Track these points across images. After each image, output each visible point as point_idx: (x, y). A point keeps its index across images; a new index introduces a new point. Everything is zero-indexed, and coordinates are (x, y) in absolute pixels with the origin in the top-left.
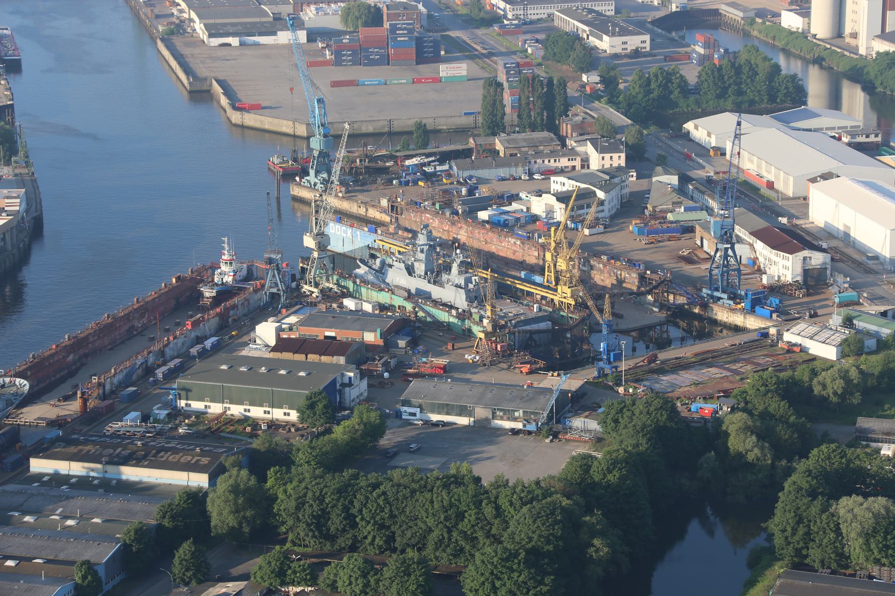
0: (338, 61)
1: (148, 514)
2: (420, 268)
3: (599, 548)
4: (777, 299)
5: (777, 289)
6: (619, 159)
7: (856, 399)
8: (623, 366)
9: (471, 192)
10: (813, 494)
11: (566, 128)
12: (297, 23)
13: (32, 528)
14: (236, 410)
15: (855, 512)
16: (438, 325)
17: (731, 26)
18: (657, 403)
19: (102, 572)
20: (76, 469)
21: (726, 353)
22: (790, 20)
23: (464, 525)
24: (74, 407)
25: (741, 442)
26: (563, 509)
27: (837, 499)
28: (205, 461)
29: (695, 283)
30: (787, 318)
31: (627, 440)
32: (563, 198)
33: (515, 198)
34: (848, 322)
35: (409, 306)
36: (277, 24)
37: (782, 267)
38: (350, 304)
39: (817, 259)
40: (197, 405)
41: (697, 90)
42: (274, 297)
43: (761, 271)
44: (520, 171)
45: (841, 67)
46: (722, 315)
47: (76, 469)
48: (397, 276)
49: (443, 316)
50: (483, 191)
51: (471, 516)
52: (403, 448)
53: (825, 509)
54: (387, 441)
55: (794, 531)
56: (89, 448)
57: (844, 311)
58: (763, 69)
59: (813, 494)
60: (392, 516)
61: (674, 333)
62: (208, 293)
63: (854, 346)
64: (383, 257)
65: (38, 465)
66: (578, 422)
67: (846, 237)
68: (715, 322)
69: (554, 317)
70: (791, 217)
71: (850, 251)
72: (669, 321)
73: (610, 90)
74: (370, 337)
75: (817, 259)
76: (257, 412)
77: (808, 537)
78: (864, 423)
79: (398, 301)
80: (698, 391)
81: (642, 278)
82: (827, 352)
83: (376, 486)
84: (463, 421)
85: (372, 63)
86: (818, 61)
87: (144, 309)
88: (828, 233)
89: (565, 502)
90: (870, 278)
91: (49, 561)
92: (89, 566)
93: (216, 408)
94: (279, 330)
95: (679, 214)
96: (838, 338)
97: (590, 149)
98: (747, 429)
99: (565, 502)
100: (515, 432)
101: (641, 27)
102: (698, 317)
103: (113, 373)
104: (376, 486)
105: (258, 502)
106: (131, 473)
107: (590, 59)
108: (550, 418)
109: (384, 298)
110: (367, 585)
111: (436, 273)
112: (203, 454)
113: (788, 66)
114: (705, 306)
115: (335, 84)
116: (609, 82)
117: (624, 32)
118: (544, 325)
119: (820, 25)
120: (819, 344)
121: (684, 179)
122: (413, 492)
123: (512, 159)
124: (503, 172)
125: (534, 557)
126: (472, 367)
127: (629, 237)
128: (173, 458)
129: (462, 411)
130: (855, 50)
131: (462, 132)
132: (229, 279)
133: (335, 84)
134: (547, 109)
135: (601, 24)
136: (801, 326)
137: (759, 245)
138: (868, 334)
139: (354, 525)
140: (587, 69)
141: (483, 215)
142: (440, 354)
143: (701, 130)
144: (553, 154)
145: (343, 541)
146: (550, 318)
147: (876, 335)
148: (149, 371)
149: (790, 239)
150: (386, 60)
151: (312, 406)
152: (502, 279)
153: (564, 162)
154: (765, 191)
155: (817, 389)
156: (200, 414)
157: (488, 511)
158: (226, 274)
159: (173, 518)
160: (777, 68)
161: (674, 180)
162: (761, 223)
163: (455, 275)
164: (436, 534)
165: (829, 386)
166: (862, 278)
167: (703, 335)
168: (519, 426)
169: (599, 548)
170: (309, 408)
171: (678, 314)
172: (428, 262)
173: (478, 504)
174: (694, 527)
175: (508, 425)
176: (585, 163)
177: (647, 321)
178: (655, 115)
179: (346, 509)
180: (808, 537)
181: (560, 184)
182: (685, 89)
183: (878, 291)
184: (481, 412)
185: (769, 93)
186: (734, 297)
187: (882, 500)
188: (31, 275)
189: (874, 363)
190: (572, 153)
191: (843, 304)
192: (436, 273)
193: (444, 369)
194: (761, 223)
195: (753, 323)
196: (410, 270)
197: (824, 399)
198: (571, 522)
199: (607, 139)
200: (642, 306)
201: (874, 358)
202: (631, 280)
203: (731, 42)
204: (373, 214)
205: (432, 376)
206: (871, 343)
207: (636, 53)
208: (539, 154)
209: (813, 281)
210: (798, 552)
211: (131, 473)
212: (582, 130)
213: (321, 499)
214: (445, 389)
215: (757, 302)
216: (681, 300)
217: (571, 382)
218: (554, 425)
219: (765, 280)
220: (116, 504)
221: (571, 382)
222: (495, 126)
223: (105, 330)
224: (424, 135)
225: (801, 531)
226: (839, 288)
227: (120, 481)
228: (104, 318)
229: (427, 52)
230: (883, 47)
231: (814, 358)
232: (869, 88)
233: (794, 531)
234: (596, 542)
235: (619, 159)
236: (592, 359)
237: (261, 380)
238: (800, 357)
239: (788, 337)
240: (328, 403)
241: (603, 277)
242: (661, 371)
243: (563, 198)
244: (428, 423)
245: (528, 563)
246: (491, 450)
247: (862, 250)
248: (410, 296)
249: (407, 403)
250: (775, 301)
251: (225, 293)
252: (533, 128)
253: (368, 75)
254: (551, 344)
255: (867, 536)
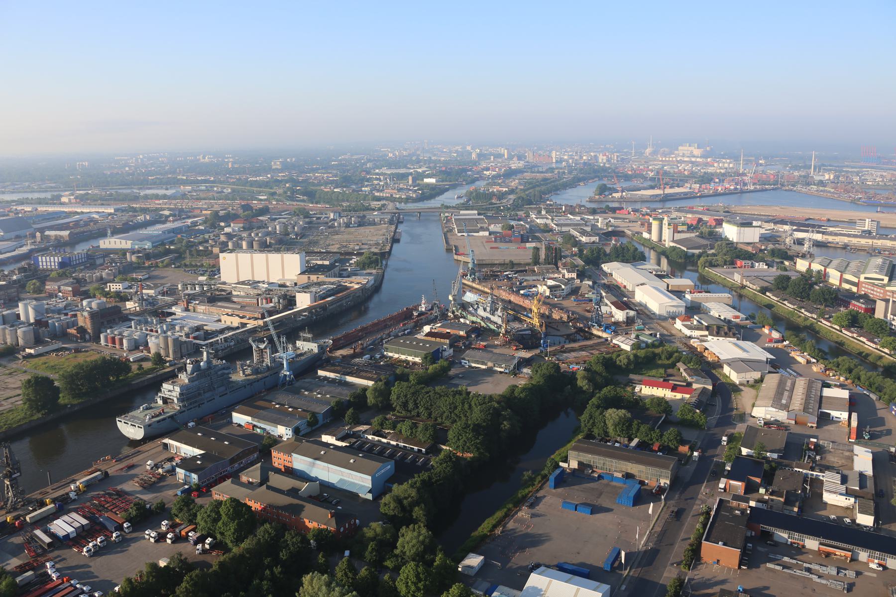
0: (495, 241)
1: (346, 395)
2: (488, 309)
3: (506, 425)
4: (616, 328)
5: (617, 324)
6: (574, 275)
7: (632, 367)
8: (549, 349)
9: (520, 284)
10: (598, 407)
11: (559, 264)
12: (487, 229)
13: (306, 396)
14: (403, 357)
15: (613, 415)
16: (491, 330)
17: (628, 236)
18: (551, 365)
19: (320, 418)
20: (332, 375)
21: (591, 346)
22: (646, 235)
23: (456, 412)
24: (352, 352)
25: (582, 383)
26: (494, 408)
27: (607, 409)
28: (375, 376)
29: (587, 319)
30: (616, 333)
31: (538, 380)
32: (550, 287)
33: (535, 286)
34: (637, 337)
35: (483, 324)
36: (482, 229)
37: (620, 315)
38: (462, 320)
39: (632, 313)
40: (390, 354)
41: (609, 255)
42: (436, 317)
43: (613, 316)
44: (541, 278)
45: (659, 251)
46: (595, 332)
47: (332, 375)
48: (481, 312)
49: (492, 327)
50: (525, 284)
51: (459, 408)
52: (456, 376)
53: (601, 414)
54: (452, 372)
55: (588, 422)
56: (339, 368)
57: (636, 333)
58: (632, 249)
59: (598, 407)
60: (431, 405)
61: (578, 337)
62: (415, 314)
63: (636, 346)
64: (481, 306)
65: (321, 373)
66: (525, 370)
67: (646, 306)
68: (592, 334)
69: (532, 329)
70: (628, 298)
71: (646, 311)
72: (576, 332)
73: (580, 254)
74: (462, 333)
75: (632, 313)
76: (410, 358)
77: (594, 424)
78: (632, 376)
79: (479, 321)
80: (575, 362)
81: (568, 317)
82: (627, 347)
83: (427, 393)
84: (484, 367)
85: (507, 242)
86: (653, 248)
87: (391, 318)
88: (640, 304)
89: (496, 405)
90: (650, 321)
91: (304, 410)
92: (314, 415)
93: (396, 356)
94: (431, 328)
95: (590, 295)
96: (632, 342)
97: (565, 271)
98: (584, 378)
99: (496, 405)
100: (501, 372)
101: (598, 235)
102: (587, 332)
103: (367, 341)
104: (427, 393)
105: (383, 393)
106: (349, 379)
107: (577, 243)
108: (514, 368)
109: (474, 319)
110: (412, 433)
111: (493, 311)
112: (376, 373)
113: (641, 249)
114: (589, 328)
115: (492, 248)
116: (581, 251)
117: (590, 236)
118: (529, 332)
119: (654, 237)
120: (625, 344)
121: (594, 283)
122: (441, 396)
123: (539, 274)
124: (534, 278)
125: (477, 428)
126: (496, 346)
127: (570, 303)
128: (364, 374)
129: (483, 363)
130: (664, 245)
131: (528, 264)
132: (423, 310)
133: (492, 248)
134: (555, 258)
135: (584, 233)
136: (620, 337)
137: (613, 307)
138: (643, 342)
139: (418, 407)
140: (575, 247)
141: (522, 292)
142: (486, 341)
143: (606, 267)
144: (553, 273)
145: (414, 413)
146: (531, 329)
147: (646, 343)
148: (382, 340)
149: (623, 305)
150: (510, 241)
151: (426, 358)
152: (515, 313)
153: (556, 275)
154: (623, 289)
155: (618, 362)
156: (391, 358)
157: (466, 406)
158: (423, 308)
159: (354, 398)
160: (636, 249)
161: (590, 283)
162: (615, 299)
163: (499, 313)
164: (445, 414)
165: (622, 361)
166: (648, 321)
167: (587, 339)
168: (502, 370)
169: (506, 425)
170: (425, 358)
171: (580, 330)
172: (491, 307)
173: (463, 404)
174: (562, 414)
175: (499, 369)
176: (563, 276)
177: (569, 332)
178: (593, 260)
179: (415, 401)
180: (594, 424)
181: (551, 283)
182: (605, 254)
183: (652, 326)
184: (490, 364)
185: (632, 256)
186: (600, 326)
187: (623, 411)
188: (371, 305)
189: (641, 353)
190: (560, 272)
191: (638, 330)
192: (493, 311)
193: (485, 346)
194: (615, 299)
195: (605, 335)
196: (485, 310)
197: (620, 366)
198: (496, 415)
199: (572, 268)
200: (568, 327)
201: (643, 351)
202: (565, 318)
203: (624, 241)
204: (486, 290)
205: (479, 349)
206: (643, 345)
207: (594, 242)
208: (548, 272)
209: (630, 321)
210: (589, 430)
211: (349, 379)
212: (565, 265)
213: (406, 396)
214: (479, 354)
215: (607, 327)
216: (582, 325)
217: (526, 354)
218: (516, 371)
219: (613, 320)
220: (339, 390)
221: (526, 354)
222: (536, 262)
223: (374, 325)
224: (512, 265)
225: (591, 421)
226: (638, 324)
227: (345, 381)
228: (376, 321)
229: (524, 239)
230: (672, 244)
231: (622, 350)
232: (667, 257)
233: (588, 422)
234: (505, 423)
235: (574, 275)
236: (537, 346)
237: (414, 348)
238: (616, 349)
239: (614, 341)
240: (434, 356)
241: (556, 316)
242: (565, 352)
243: (550, 287)
244: (470, 366)
245: (473, 430)
246: (490, 379)
247: (650, 311)
248: (483, 319)
249: (464, 359)
250: (613, 328)
251: (421, 314)
252: (549, 264)
253: (503, 246)
254: (527, 340)
255: (616, 425)
